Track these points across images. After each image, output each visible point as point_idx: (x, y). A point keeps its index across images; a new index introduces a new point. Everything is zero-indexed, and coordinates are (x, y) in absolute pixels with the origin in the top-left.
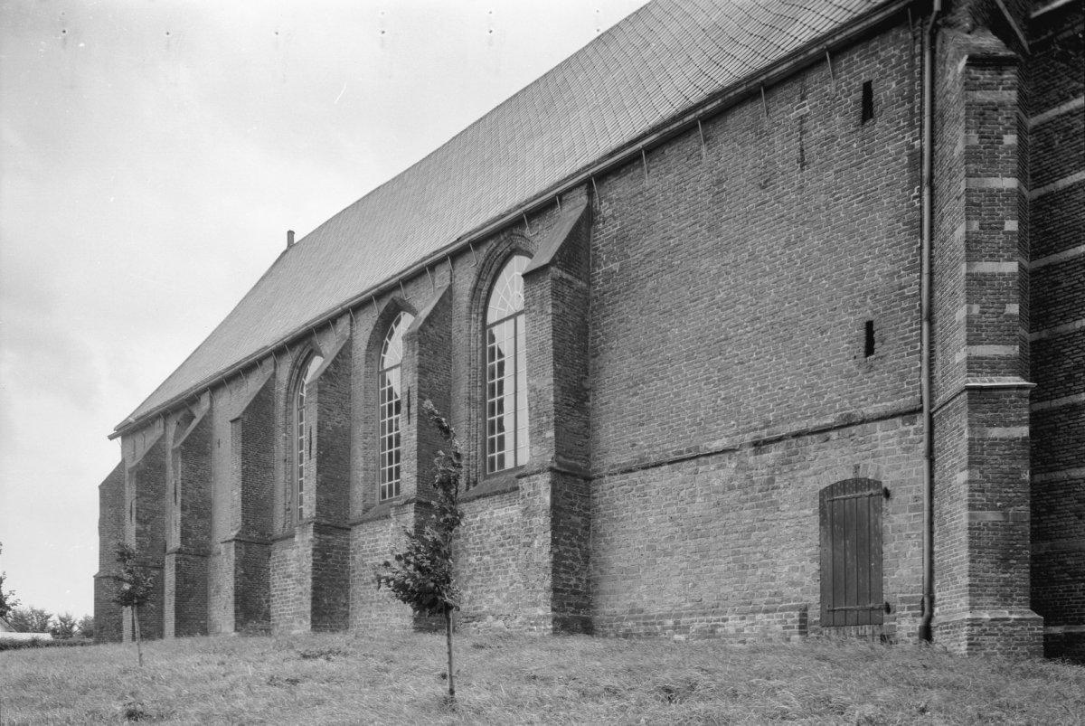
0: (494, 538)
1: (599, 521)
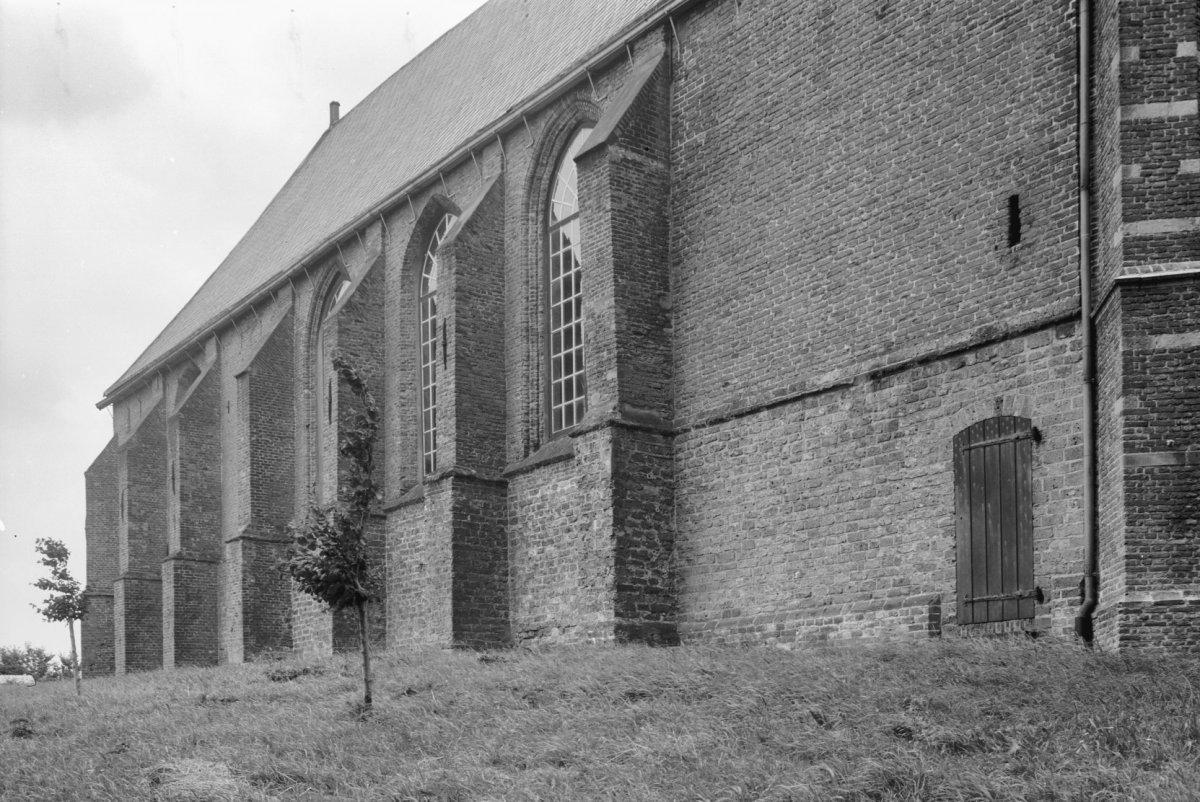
0: (558, 521)
1: (685, 491)
